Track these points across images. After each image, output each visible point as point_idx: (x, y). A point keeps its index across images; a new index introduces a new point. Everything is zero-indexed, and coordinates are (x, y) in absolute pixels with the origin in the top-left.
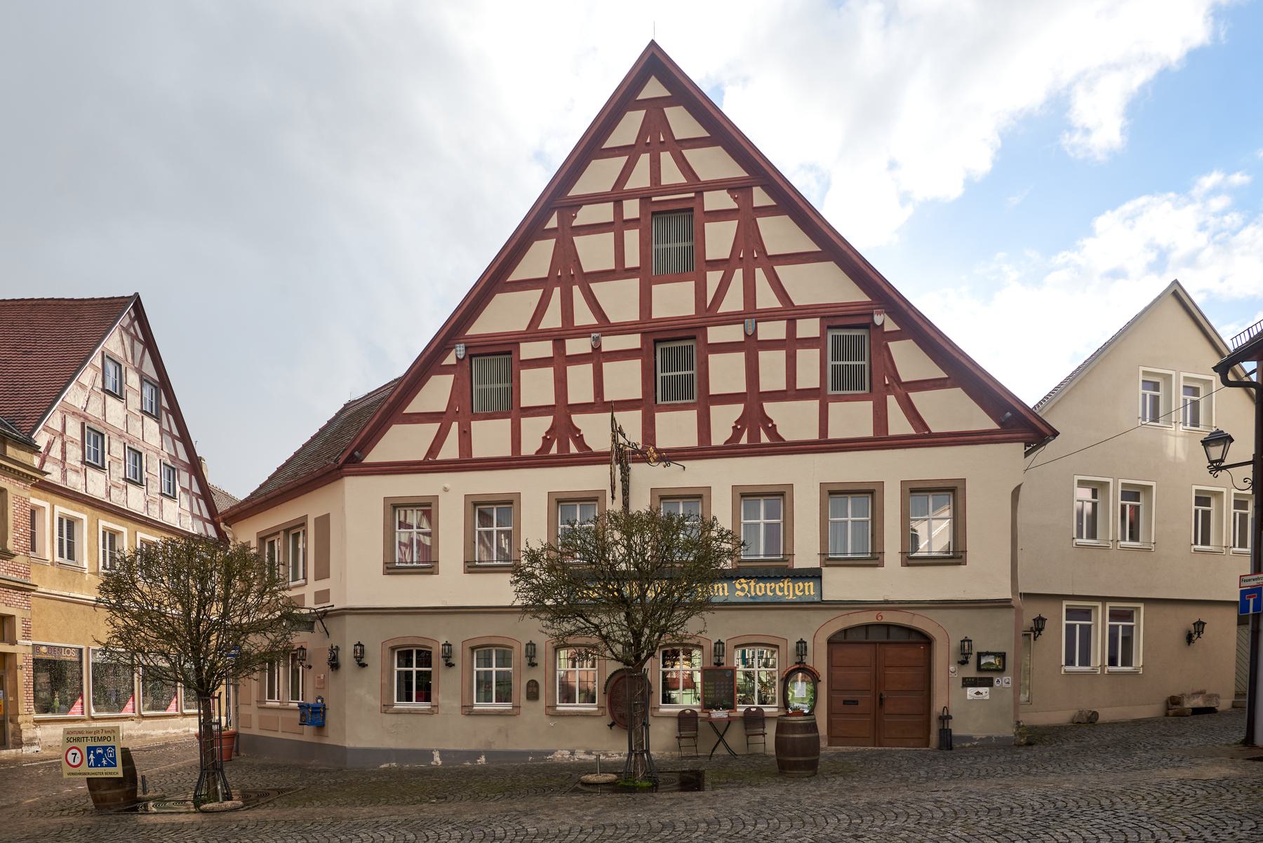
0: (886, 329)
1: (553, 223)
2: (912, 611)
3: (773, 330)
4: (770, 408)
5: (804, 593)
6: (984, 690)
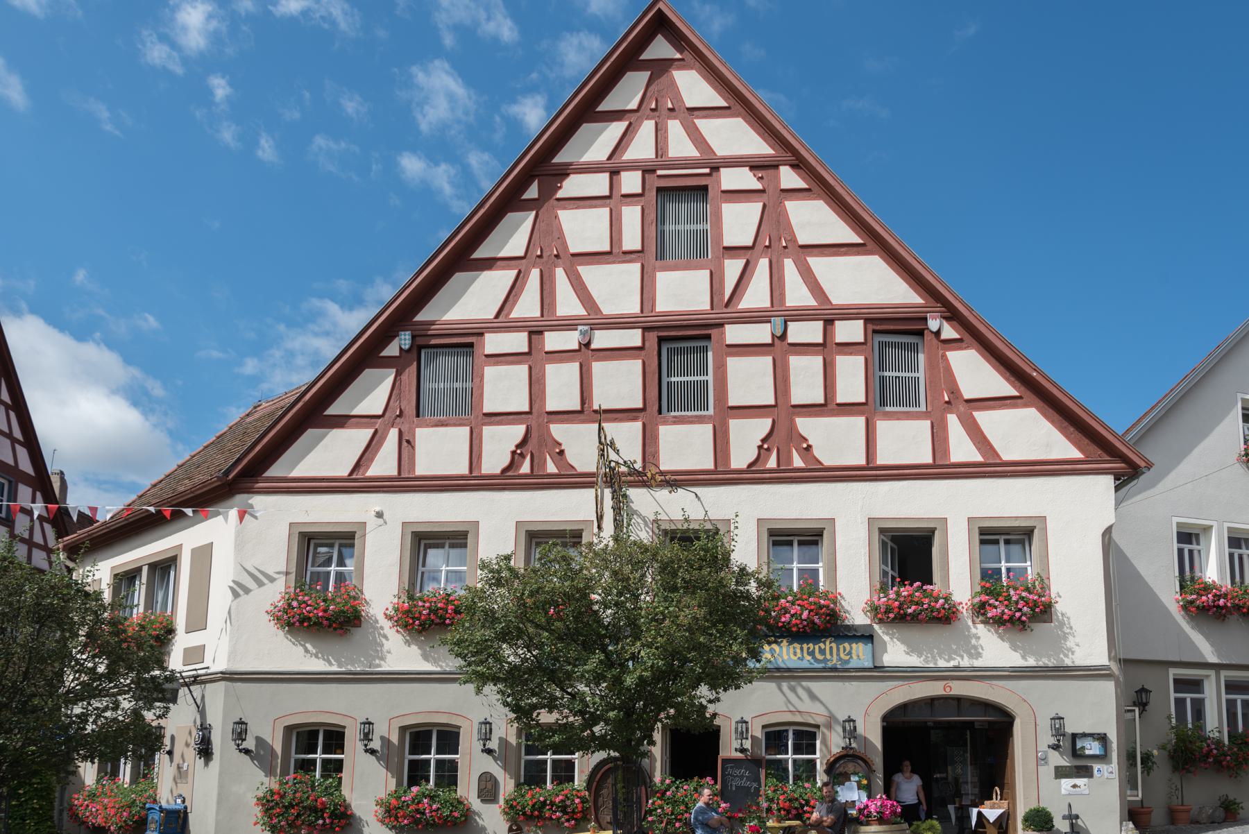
0: (944, 336)
1: (532, 192)
3: (569, 340)
4: (805, 425)
6: (1081, 782)
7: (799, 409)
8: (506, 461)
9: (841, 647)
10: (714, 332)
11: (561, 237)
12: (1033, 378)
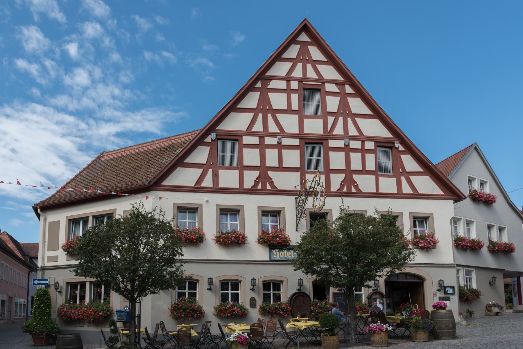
0: (400, 149)
1: (259, 85)
2: (417, 268)
3: (273, 141)
4: (355, 177)
5: (291, 256)
9: (280, 253)
10: (324, 142)
12: (430, 166)
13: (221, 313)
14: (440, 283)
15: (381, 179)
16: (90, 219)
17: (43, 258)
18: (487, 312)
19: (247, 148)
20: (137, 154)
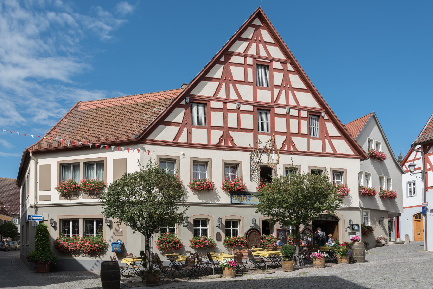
0: (325, 118)
1: (223, 59)
7: (292, 134)
8: (218, 141)
10: (272, 109)
11: (231, 74)
13: (196, 245)
14: (350, 222)
15: (311, 141)
16: (81, 165)
17: (36, 198)
18: (377, 243)
19: (214, 111)
20: (115, 108)
